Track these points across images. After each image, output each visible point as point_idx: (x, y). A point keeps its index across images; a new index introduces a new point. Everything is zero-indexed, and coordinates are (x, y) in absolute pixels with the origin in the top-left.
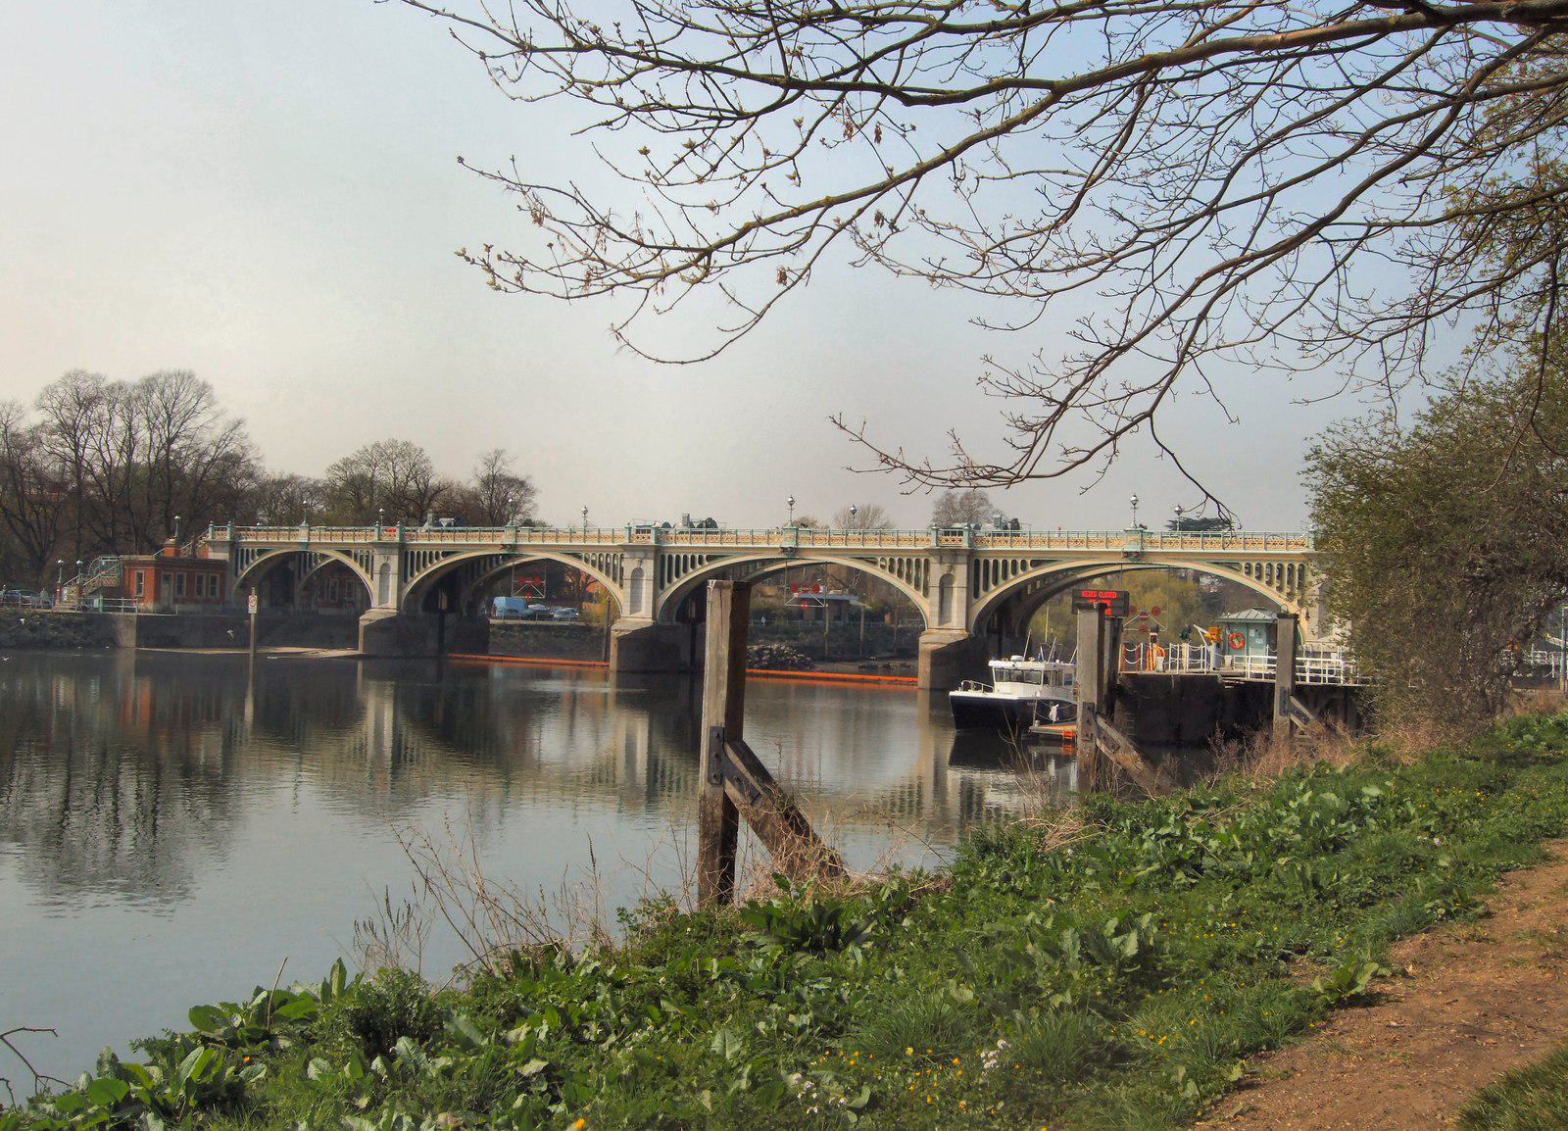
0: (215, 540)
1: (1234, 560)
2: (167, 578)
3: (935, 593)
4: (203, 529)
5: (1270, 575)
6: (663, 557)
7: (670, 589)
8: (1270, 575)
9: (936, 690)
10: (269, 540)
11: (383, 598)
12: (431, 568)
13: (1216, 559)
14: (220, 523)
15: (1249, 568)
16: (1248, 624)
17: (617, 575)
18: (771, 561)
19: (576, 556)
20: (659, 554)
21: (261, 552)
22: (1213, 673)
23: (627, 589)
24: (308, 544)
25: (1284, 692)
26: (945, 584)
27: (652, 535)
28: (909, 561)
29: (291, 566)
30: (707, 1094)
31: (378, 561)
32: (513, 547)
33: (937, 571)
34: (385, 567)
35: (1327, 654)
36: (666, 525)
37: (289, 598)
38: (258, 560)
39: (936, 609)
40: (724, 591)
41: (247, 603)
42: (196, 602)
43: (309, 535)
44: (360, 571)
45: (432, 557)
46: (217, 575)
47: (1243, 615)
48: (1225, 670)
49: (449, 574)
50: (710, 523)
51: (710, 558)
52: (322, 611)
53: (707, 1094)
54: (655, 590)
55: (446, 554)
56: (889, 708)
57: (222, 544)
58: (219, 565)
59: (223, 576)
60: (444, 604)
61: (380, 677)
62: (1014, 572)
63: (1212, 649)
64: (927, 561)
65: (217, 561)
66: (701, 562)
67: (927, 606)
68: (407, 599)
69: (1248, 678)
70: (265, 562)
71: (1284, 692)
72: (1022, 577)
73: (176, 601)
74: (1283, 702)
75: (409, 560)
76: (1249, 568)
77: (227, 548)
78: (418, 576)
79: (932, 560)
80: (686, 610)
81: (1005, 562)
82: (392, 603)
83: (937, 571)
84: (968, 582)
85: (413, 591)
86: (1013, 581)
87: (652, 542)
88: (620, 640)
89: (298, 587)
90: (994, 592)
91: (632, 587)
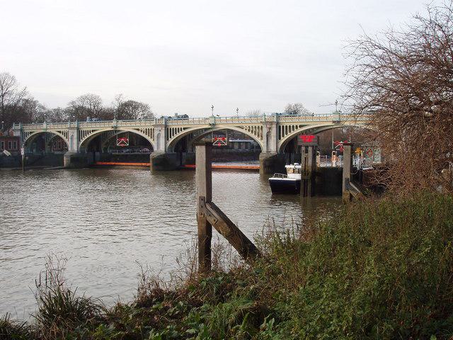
0: (16, 130)
3: (265, 138)
4: (11, 126)
6: (280, 127)
10: (36, 129)
12: (176, 136)
14: (17, 123)
19: (138, 130)
23: (156, 141)
25: (347, 180)
26: (268, 136)
30: (180, 302)
31: (156, 133)
32: (116, 127)
37: (43, 148)
38: (30, 135)
39: (265, 144)
41: (20, 151)
44: (64, 138)
49: (95, 138)
50: (186, 117)
52: (56, 153)
53: (180, 302)
56: (134, 173)
57: (18, 130)
58: (17, 138)
60: (95, 148)
62: (293, 130)
67: (262, 143)
68: (81, 148)
71: (347, 180)
72: (181, 133)
74: (347, 184)
75: (80, 134)
78: (173, 138)
82: (75, 149)
83: (265, 131)
86: (293, 133)
88: (153, 159)
89: (47, 144)
90: (286, 137)
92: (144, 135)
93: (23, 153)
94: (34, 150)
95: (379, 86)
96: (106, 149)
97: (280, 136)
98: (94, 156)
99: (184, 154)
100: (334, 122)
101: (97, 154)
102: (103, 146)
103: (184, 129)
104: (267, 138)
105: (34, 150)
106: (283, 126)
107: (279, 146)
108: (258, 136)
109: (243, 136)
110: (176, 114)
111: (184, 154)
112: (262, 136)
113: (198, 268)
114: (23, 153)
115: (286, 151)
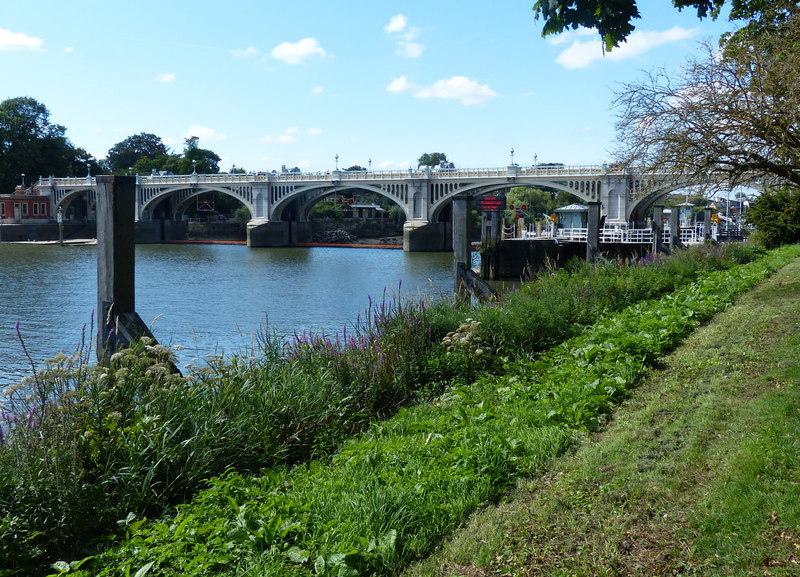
1: (564, 180)
2: (17, 206)
3: (411, 203)
4: (36, 180)
5: (583, 187)
7: (276, 204)
8: (583, 187)
9: (163, 238)
12: (284, 198)
13: (555, 180)
14: (45, 176)
15: (571, 184)
16: (571, 213)
17: (249, 197)
18: (329, 188)
19: (228, 188)
20: (630, 181)
21: (162, 189)
22: (553, 238)
27: (266, 177)
28: (398, 186)
29: (85, 198)
31: (255, 193)
33: (411, 192)
34: (260, 197)
35: (613, 227)
36: (274, 171)
42: (34, 217)
47: (569, 208)
48: (561, 236)
51: (296, 187)
55: (162, 189)
56: (213, 247)
58: (46, 199)
59: (48, 204)
60: (163, 215)
63: (552, 225)
67: (407, 209)
70: (70, 196)
72: (291, 194)
73: (23, 217)
76: (571, 184)
78: (280, 201)
79: (409, 185)
80: (444, 213)
81: (446, 185)
83: (411, 192)
85: (146, 209)
87: (266, 180)
92: (237, 197)
93: (60, 220)
94: (71, 217)
95: (457, 461)
96: (179, 216)
97: (432, 199)
98: (163, 227)
99: (294, 223)
101: (167, 222)
102: (175, 211)
104: (415, 201)
105: (71, 217)
106: (442, 185)
107: (430, 216)
108: (402, 198)
109: (380, 199)
110: (284, 168)
111: (294, 223)
112: (406, 199)
113: (532, 239)
114: (60, 220)
115: (284, 217)
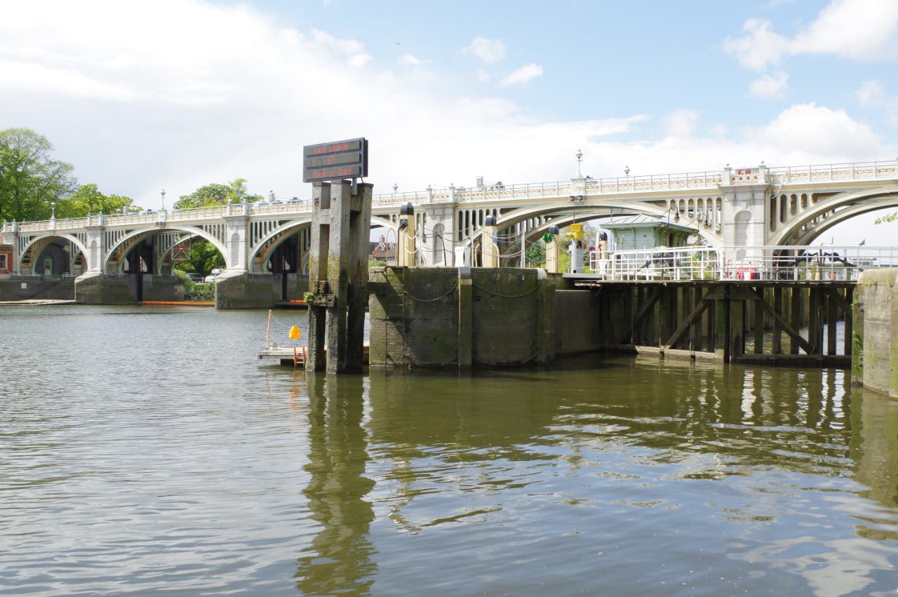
11: (94, 265)
12: (270, 235)
21: (31, 238)
23: (230, 249)
24: (54, 231)
31: (230, 233)
34: (236, 238)
40: (451, 235)
43: (55, 225)
45: (270, 226)
46: (7, 255)
54: (246, 248)
61: (544, 280)
64: (223, 226)
65: (8, 245)
66: (805, 204)
69: (648, 280)
77: (13, 237)
84: (454, 229)
91: (233, 247)
100: (573, 198)
103: (281, 223)
